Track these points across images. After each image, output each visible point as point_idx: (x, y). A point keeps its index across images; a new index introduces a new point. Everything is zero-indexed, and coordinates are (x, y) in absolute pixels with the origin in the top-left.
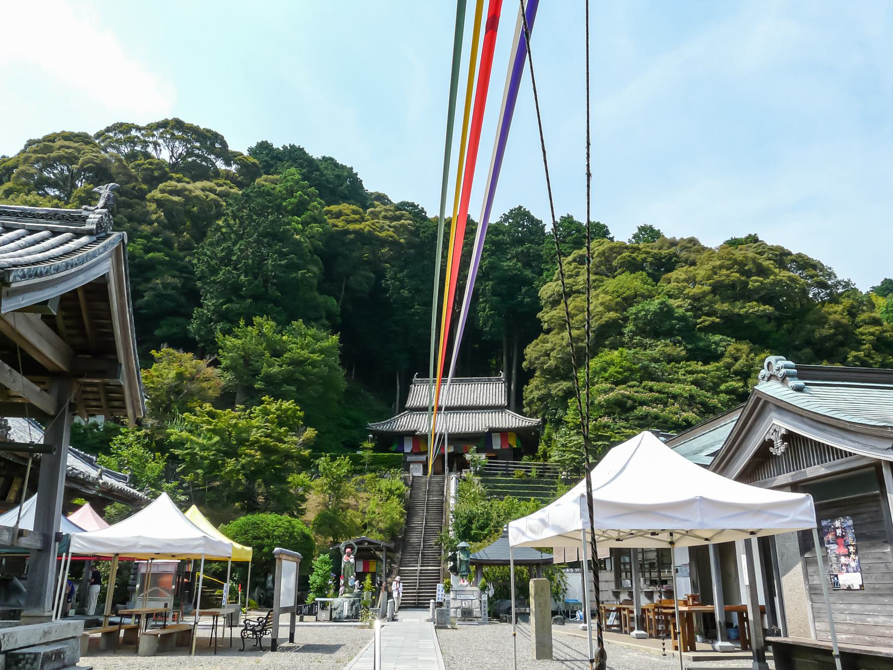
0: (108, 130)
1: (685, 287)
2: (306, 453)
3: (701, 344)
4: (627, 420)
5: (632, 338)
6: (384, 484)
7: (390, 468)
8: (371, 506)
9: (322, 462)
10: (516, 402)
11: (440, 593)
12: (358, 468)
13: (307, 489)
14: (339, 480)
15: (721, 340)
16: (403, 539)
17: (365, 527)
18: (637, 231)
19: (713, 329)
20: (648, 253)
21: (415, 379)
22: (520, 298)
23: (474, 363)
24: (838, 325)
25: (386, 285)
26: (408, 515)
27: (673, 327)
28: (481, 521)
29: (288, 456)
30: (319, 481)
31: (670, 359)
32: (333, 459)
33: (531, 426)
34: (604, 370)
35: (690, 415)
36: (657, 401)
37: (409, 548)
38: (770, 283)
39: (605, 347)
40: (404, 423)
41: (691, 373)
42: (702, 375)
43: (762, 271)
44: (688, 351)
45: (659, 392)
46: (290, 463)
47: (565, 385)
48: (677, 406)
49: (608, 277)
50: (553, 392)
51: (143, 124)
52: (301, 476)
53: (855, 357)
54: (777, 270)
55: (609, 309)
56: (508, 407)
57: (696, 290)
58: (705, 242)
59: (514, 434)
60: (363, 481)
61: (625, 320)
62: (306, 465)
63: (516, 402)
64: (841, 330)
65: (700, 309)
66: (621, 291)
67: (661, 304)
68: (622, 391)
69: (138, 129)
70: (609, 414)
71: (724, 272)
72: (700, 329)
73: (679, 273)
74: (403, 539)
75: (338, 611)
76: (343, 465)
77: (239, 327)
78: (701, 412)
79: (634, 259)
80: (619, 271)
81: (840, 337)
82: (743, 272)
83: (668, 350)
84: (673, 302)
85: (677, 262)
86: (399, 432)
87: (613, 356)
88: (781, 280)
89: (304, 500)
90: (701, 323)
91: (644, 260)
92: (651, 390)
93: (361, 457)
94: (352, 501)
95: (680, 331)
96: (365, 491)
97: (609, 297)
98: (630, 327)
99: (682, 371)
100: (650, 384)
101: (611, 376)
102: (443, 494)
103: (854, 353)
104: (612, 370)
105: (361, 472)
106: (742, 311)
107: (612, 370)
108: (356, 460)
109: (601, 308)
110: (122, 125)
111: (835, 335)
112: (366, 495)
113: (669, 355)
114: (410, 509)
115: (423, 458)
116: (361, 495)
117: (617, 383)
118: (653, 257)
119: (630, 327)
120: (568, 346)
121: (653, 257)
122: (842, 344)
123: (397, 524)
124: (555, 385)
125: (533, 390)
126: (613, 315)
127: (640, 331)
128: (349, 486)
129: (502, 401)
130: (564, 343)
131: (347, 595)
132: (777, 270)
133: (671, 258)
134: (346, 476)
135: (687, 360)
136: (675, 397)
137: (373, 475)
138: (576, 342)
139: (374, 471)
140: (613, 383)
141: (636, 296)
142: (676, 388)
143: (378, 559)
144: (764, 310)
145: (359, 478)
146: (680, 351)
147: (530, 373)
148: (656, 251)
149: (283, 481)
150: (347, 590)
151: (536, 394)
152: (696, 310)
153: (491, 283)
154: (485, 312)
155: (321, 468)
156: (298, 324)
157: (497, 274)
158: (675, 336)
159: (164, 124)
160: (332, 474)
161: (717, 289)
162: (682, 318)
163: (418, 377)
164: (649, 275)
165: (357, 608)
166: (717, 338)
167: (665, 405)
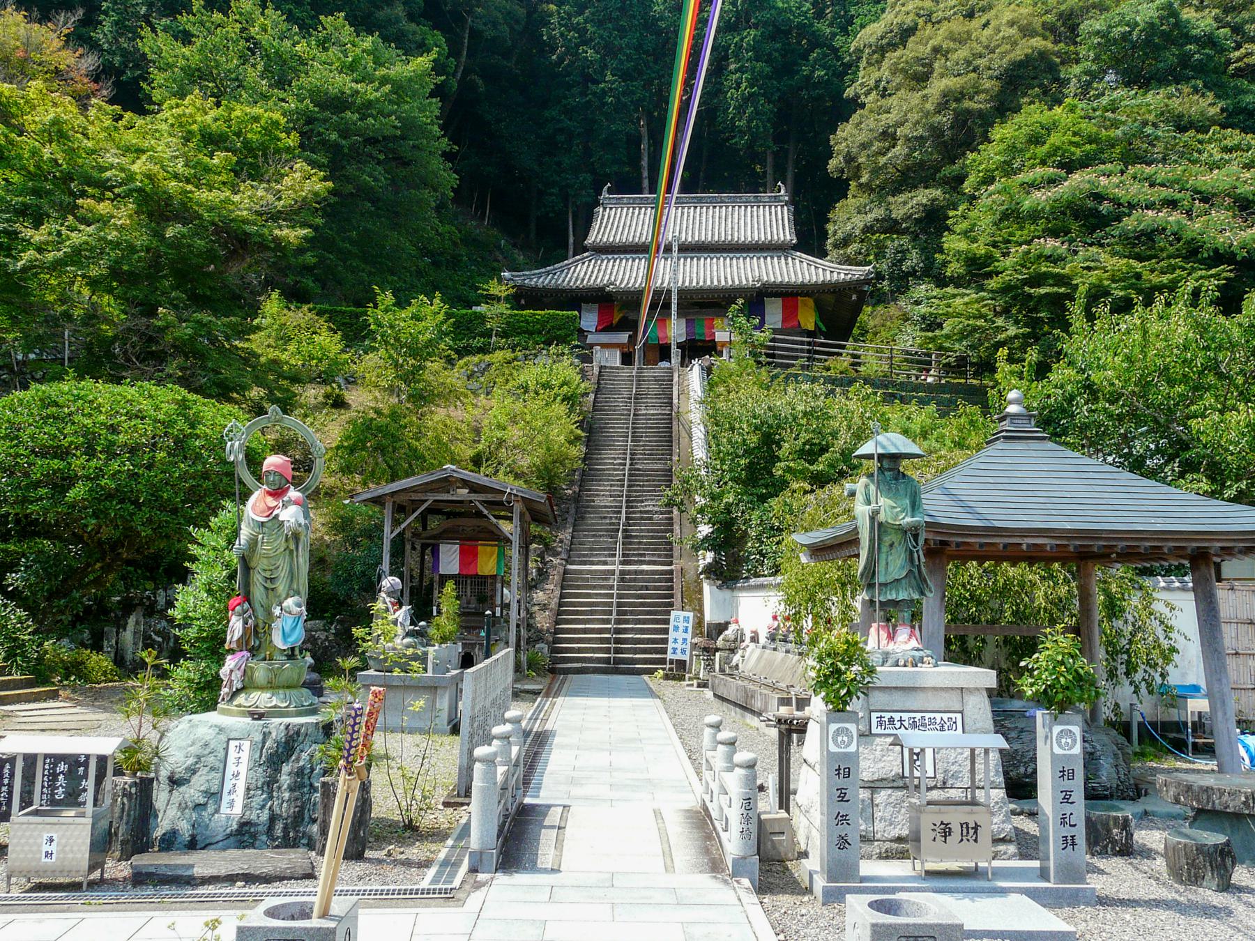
6: (531, 373)
7: (548, 343)
10: (810, 238)
11: (680, 635)
16: (577, 499)
21: (605, 194)
22: (805, 70)
23: (719, 169)
25: (550, 37)
26: (589, 442)
28: (805, 436)
33: (850, 282)
36: (1172, 204)
37: (591, 520)
40: (583, 273)
55: (1027, 31)
56: (796, 248)
59: (811, 302)
63: (810, 238)
70: (1054, 234)
72: (1239, 73)
74: (577, 499)
75: (192, 792)
77: (190, 12)
86: (571, 290)
90: (1240, 59)
93: (482, 318)
101: (1055, 150)
102: (671, 404)
109: (1013, 31)
113: (1180, 116)
114: (592, 432)
115: (624, 337)
117: (1069, 167)
123: (561, 460)
124: (901, 198)
125: (849, 216)
129: (786, 234)
131: (262, 699)
135: (1224, 127)
138: (957, 100)
140: (1061, 166)
143: (503, 540)
147: (839, 189)
150: (261, 671)
151: (859, 222)
153: (753, 32)
154: (738, 85)
156: (335, 23)
157: (766, 15)
163: (610, 191)
165: (302, 780)
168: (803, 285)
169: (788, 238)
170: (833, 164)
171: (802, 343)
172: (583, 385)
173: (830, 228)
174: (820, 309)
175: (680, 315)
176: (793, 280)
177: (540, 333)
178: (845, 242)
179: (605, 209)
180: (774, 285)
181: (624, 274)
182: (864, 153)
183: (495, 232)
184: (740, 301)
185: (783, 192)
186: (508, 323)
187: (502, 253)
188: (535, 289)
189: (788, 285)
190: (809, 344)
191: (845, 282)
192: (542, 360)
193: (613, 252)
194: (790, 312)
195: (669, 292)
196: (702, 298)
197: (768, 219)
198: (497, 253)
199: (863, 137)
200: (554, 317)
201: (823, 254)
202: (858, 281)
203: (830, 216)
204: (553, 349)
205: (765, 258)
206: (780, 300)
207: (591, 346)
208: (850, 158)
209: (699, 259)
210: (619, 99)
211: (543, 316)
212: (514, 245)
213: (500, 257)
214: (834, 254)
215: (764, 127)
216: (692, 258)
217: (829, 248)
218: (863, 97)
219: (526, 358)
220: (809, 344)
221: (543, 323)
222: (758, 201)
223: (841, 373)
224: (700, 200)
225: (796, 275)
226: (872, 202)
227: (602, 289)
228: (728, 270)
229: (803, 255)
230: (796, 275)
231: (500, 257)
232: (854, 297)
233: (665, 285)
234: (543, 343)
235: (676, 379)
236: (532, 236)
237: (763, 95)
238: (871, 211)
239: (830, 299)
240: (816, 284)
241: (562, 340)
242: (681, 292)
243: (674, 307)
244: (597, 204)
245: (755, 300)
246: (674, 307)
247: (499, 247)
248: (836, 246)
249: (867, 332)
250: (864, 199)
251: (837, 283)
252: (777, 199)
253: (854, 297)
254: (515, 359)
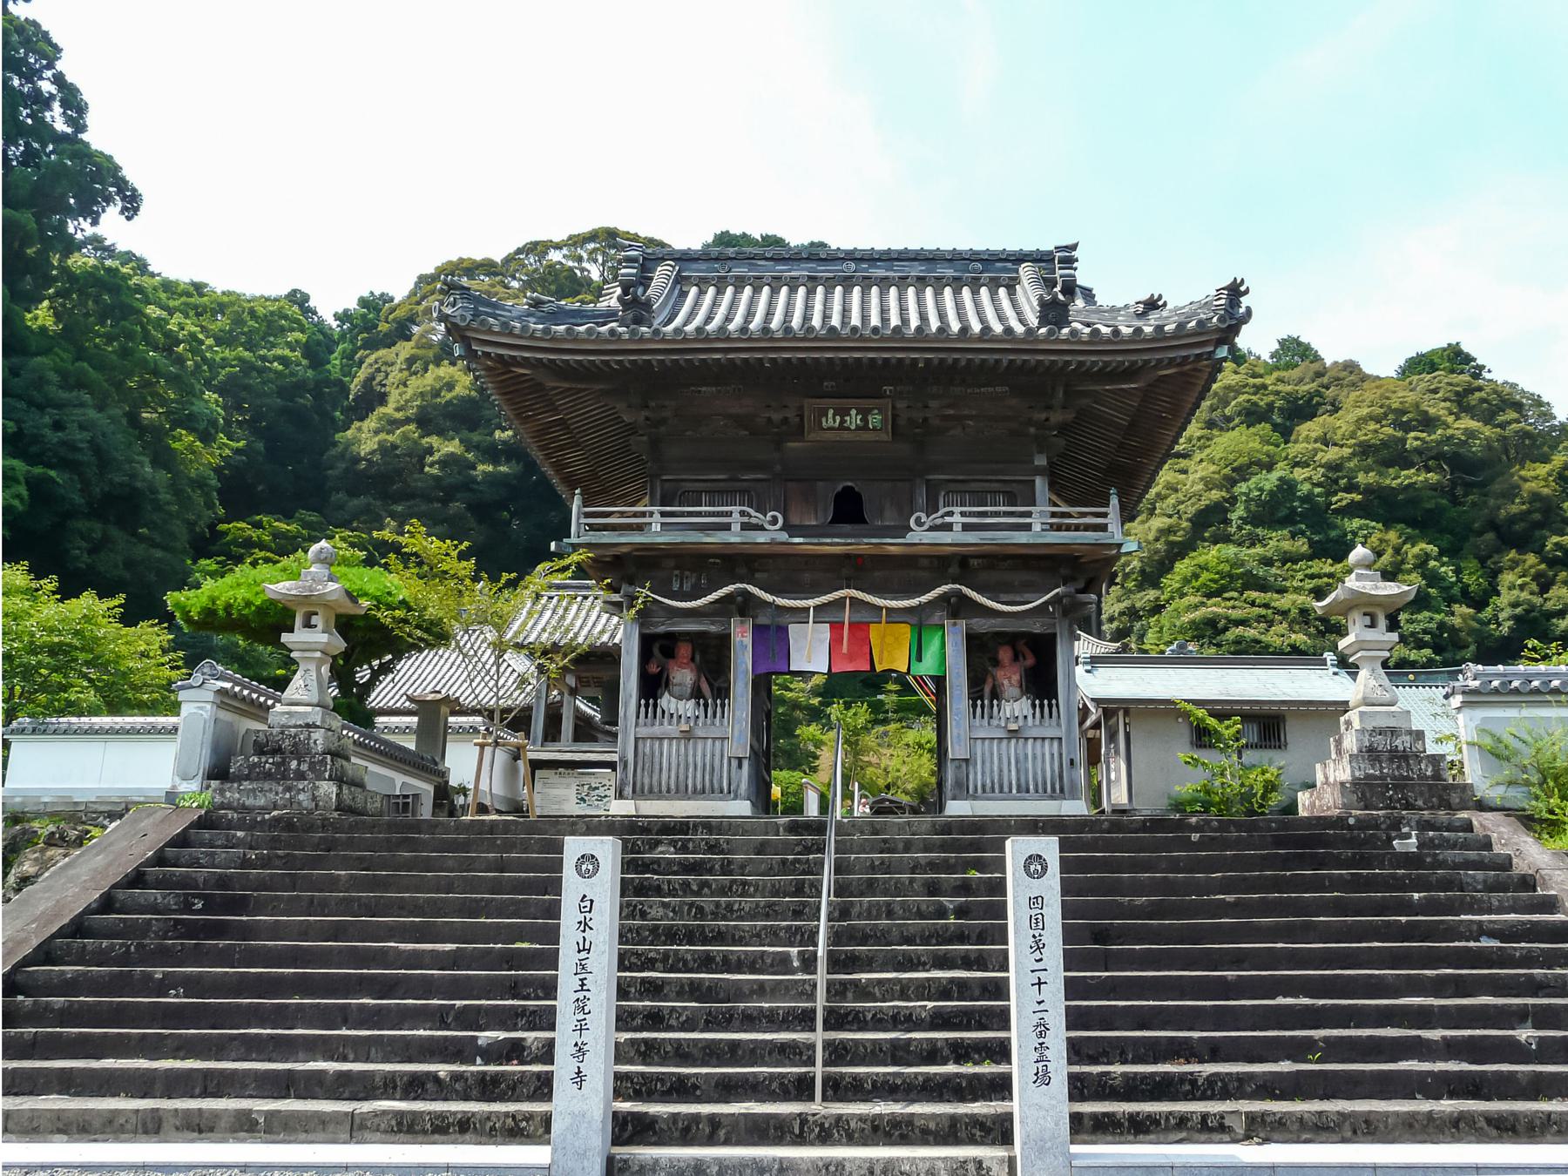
0: (519, 251)
1: (1316, 451)
2: (815, 701)
3: (1333, 534)
4: (1219, 645)
5: (1240, 528)
6: (911, 736)
8: (894, 764)
9: (835, 711)
12: (881, 716)
13: (819, 744)
14: (856, 732)
15: (1361, 528)
17: (888, 787)
18: (1277, 346)
19: (1351, 510)
20: (1277, 393)
24: (1536, 497)
27: (1293, 510)
29: (795, 705)
30: (832, 734)
31: (1288, 558)
32: (848, 706)
34: (1196, 576)
35: (1299, 638)
38: (1436, 441)
39: (1204, 540)
41: (1312, 577)
42: (1325, 580)
43: (1428, 423)
44: (1311, 543)
45: (1266, 606)
46: (798, 713)
47: (1152, 594)
48: (1285, 625)
49: (1221, 429)
50: (1138, 605)
51: (558, 237)
52: (811, 729)
53: (1556, 544)
54: (1450, 419)
57: (1332, 454)
58: (1368, 368)
60: (886, 734)
61: (1233, 500)
62: (816, 715)
64: (1538, 505)
65: (1336, 482)
66: (1231, 457)
67: (1280, 479)
68: (1215, 608)
69: (558, 247)
71: (1372, 426)
72: (1336, 511)
73: (1309, 429)
76: (860, 714)
78: (1320, 632)
79: (1255, 404)
80: (1237, 421)
81: (1537, 516)
82: (1397, 424)
83: (1286, 545)
84: (1299, 474)
85: (1319, 404)
87: (1212, 554)
88: (1452, 436)
89: (816, 757)
91: (1271, 406)
92: (1253, 604)
94: (874, 760)
95: (1304, 517)
96: (889, 746)
97: (1213, 468)
98: (1239, 512)
99: (1300, 576)
100: (1254, 594)
103: (1555, 539)
104: (1205, 576)
105: (885, 722)
106: (1394, 484)
107: (1205, 576)
108: (876, 707)
110: (536, 244)
111: (1529, 512)
112: (891, 751)
116: (884, 751)
117: (1209, 596)
118: (1283, 398)
119: (1239, 512)
120: (1157, 539)
121: (1283, 398)
122: (1540, 525)
123: (927, 785)
126: (1216, 495)
127: (1254, 519)
128: (869, 740)
130: (1151, 537)
132: (1450, 419)
133: (1311, 399)
134: (865, 728)
135: (1310, 558)
136: (1284, 613)
137: (898, 725)
139: (900, 720)
141: (1251, 464)
142: (1284, 602)
144: (1427, 480)
145: (881, 729)
146: (1301, 545)
148: (1289, 388)
149: (790, 733)
151: (1118, 608)
152: (1331, 486)
155: (833, 718)
158: (1294, 523)
159: (593, 236)
160: (848, 725)
161: (1365, 450)
162: (1308, 498)
164: (1275, 427)
166: (1356, 523)
167: (1271, 623)
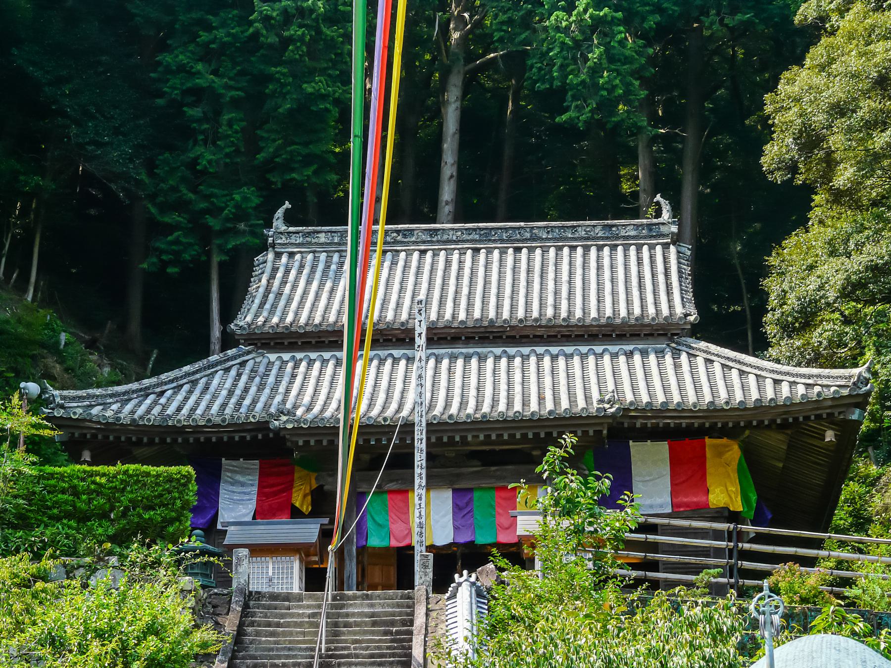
7: (121, 539)
10: (729, 312)
21: (279, 223)
23: (514, 163)
33: (819, 403)
56: (700, 331)
59: (734, 452)
63: (729, 312)
125: (809, 266)
129: (677, 304)
147: (789, 208)
151: (834, 273)
168: (713, 410)
169: (679, 310)
170: (773, 154)
171: (717, 535)
172: (198, 636)
173: (773, 285)
174: (754, 466)
175: (433, 482)
176: (692, 398)
177: (104, 515)
178: (806, 319)
179: (278, 255)
180: (650, 411)
181: (310, 392)
182: (841, 123)
183: (47, 315)
184: (569, 439)
185: (666, 215)
186: (29, 497)
187: (62, 361)
188: (111, 427)
189: (680, 411)
190: (730, 536)
191: (806, 402)
192: (101, 579)
193: (292, 347)
194: (688, 472)
195: (408, 428)
196: (500, 440)
197: (636, 271)
198: (50, 361)
199: (837, 91)
200: (138, 480)
201: (759, 345)
202: (837, 400)
203: (773, 260)
204: (135, 552)
205: (629, 355)
206: (663, 448)
207: (231, 548)
208: (810, 141)
209: (482, 359)
210: (319, 32)
211: (111, 478)
212: (91, 345)
213: (57, 369)
214: (781, 347)
215: (627, 85)
216: (467, 358)
217: (771, 330)
218: (834, 17)
219: (69, 572)
220: (730, 536)
221: (113, 493)
222: (612, 239)
223: (804, 600)
224: (486, 236)
225: (698, 389)
226: (861, 229)
227: (263, 426)
228: (548, 381)
229: (713, 348)
230: (698, 389)
231: (57, 369)
232: (830, 436)
233: (405, 413)
234: (112, 539)
235: (420, 619)
236: (135, 326)
237: (621, 22)
238: (859, 246)
239: (777, 441)
240: (742, 408)
241: (155, 533)
242: (433, 428)
243: (420, 458)
244: (264, 247)
245: (608, 442)
246: (420, 458)
247: (53, 348)
248: (788, 330)
249: (869, 521)
250: (846, 222)
251: (789, 406)
252: (653, 232)
253: (830, 436)
254: (44, 577)
